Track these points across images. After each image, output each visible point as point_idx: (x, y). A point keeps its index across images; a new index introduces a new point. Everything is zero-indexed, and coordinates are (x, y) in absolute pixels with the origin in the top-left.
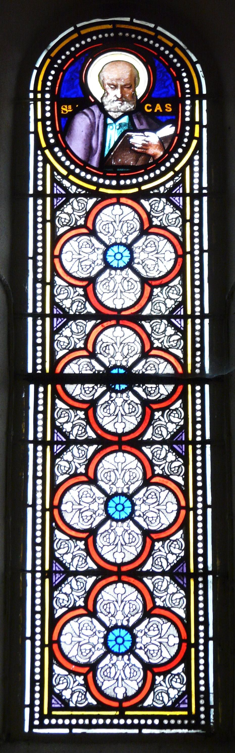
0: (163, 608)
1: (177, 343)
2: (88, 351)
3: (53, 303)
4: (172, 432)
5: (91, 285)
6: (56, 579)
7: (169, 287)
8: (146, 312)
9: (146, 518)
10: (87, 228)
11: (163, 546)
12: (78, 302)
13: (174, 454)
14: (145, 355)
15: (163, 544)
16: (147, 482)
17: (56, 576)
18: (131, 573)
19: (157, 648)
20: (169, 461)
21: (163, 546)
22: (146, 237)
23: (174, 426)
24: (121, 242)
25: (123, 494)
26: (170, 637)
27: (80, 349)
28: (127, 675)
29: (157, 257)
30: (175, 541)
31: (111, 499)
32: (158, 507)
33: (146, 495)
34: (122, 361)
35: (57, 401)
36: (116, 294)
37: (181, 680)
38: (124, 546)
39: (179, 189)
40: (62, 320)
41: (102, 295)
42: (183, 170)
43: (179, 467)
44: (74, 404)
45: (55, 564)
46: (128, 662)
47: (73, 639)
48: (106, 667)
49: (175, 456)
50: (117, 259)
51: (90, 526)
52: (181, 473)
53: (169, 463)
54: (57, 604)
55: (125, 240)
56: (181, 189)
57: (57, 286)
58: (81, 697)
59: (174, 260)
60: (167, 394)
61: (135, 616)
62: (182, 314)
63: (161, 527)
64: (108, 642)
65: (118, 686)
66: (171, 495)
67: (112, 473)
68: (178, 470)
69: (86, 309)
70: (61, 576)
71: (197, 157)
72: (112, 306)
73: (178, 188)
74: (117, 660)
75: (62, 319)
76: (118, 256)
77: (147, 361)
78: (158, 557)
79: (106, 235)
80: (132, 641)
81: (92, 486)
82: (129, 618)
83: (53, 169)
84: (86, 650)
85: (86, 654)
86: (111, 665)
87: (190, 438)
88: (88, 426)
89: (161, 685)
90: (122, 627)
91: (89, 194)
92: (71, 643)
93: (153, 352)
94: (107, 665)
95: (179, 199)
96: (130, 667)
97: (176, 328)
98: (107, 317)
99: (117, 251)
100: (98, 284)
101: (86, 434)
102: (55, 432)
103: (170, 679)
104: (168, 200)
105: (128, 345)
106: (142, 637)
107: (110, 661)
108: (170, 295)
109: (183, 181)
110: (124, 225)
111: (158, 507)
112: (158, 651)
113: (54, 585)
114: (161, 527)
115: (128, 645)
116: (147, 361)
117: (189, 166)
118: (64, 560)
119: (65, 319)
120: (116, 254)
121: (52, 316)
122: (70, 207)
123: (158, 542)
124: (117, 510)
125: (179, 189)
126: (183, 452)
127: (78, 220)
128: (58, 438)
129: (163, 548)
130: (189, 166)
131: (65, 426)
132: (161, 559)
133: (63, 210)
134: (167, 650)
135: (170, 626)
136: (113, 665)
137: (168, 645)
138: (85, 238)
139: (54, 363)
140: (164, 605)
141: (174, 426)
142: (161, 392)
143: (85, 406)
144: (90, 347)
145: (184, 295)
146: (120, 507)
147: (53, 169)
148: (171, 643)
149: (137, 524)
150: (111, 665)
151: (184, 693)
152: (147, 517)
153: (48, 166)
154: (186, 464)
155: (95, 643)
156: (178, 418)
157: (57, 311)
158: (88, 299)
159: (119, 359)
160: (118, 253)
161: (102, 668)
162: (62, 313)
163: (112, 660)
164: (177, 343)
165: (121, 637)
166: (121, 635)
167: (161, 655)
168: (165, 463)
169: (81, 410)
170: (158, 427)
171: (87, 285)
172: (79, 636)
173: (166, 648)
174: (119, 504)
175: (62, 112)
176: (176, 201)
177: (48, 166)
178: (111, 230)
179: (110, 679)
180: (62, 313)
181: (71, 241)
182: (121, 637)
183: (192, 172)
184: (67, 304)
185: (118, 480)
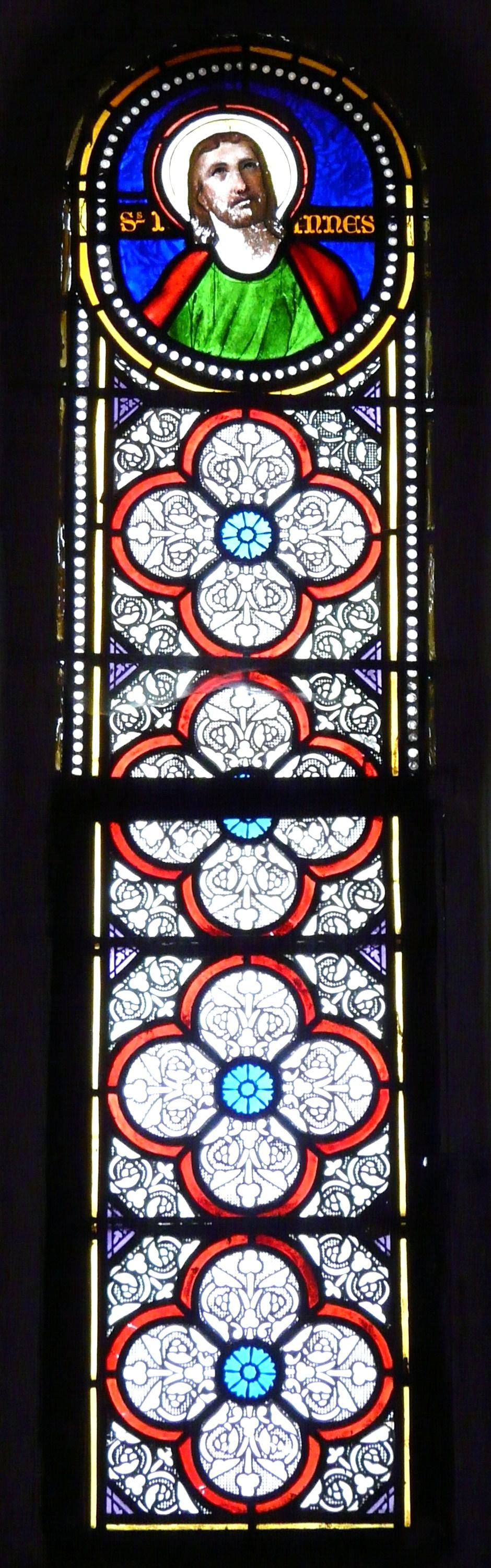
0: (333, 735)
1: (368, 721)
2: (183, 473)
3: (108, 630)
4: (353, 648)
5: (189, 595)
6: (117, 963)
7: (350, 603)
8: (303, 654)
9: (302, 555)
10: (181, 1156)
11: (334, 614)
12: (161, 632)
13: (359, 691)
14: (300, 746)
15: (335, 610)
16: (301, 484)
17: (113, 1236)
18: (273, 1228)
19: (320, 549)
20: (349, 704)
21: (334, 614)
22: (311, 1327)
23: (358, 636)
24: (256, 1407)
25: (253, 508)
26: (345, 526)
27: (168, 470)
28: (262, 1159)
29: (329, 533)
30: (366, 883)
31: (230, 1071)
32: (326, 533)
33: (300, 509)
34: (252, 758)
35: (116, 581)
36: (241, 615)
37: (367, 613)
38: (257, 613)
39: (375, 653)
40: (126, 669)
41: (211, 617)
42: (381, 351)
43: (369, 717)
44: (153, 872)
45: (114, 644)
46: (267, 1421)
47: (154, 533)
48: (220, 1430)
49: (360, 694)
50: (245, 1097)
51: (186, 572)
52: (373, 728)
53: (348, 708)
54: (120, 464)
55: (260, 761)
56: (378, 391)
57: (118, 597)
58: (168, 641)
59: (370, 1098)
60: (349, 565)
61: (279, 487)
62: (379, 658)
63: (332, 572)
64: (224, 1092)
65: (243, 1472)
66: (351, 509)
67: (232, 465)
68: (367, 723)
69: (179, 646)
70: (124, 1236)
71: (392, 348)
72: (231, 639)
73: (373, 389)
74: (243, 1417)
75: (127, 665)
76: (250, 1371)
77: (304, 496)
78: (324, 635)
79: (221, 1037)
80: (277, 1374)
81: (190, 493)
82: (267, 490)
83: (114, 350)
84: (177, 1395)
85: (179, 1120)
86: (229, 1427)
87: (394, 657)
88: (181, 633)
89: (333, 903)
90: (253, 508)
91: (180, 400)
92: (149, 542)
93: (317, 742)
94: (222, 1426)
95: (375, 413)
96: (269, 1432)
97: (366, 430)
98: (224, 665)
99: (245, 546)
100: (203, 593)
101: (177, 648)
102: (106, 1495)
103: (352, 890)
104: (352, 416)
105: (269, 463)
106: (288, 529)
107: (228, 1417)
108: (353, 620)
109: (382, 374)
110: (260, 468)
111: (326, 533)
112: (324, 554)
113: (112, 640)
114: (332, 572)
115: (268, 1381)
116: (304, 496)
117: (393, 342)
118: (130, 637)
119: (134, 667)
120: (243, 1367)
121: (109, 394)
122: (143, 429)
123: (336, 1448)
124: (242, 541)
125: (374, 392)
126: (378, 687)
127: (161, 458)
128: (115, 1507)
129: (340, 897)
130: (393, 342)
131: (130, 1482)
132: (338, 1194)
133: (129, 435)
134: (347, 1107)
135: (345, 505)
136: (233, 1425)
137: (343, 542)
138: (179, 493)
139: (109, 759)
140: (336, 727)
141: (358, 636)
142: (336, 562)
143: (174, 1151)
144: (188, 467)
145: (384, 620)
146: (247, 535)
147: (114, 350)
148: (358, 1380)
149: (282, 567)
150: (229, 1427)
151: (374, 639)
152: (303, 552)
153: (102, 343)
154: (384, 711)
155: (198, 539)
156: (366, 620)
157: (116, 648)
158: (182, 625)
159: (245, 757)
160: (250, 1364)
161: (210, 1432)
162: (125, 652)
163: (232, 1416)
164: (368, 721)
165: (251, 541)
166: (253, 1361)
167: (331, 563)
168: (341, 709)
169: (166, 598)
170: (328, 918)
171: (180, 1153)
172: (165, 528)
173: (339, 547)
174: (249, 542)
175: (124, 229)
176: (373, 959)
177: (102, 343)
178: (233, 475)
179: (226, 1456)
180: (125, 652)
181: (147, 501)
182: (251, 541)
183: (402, 351)
184: (138, 635)
185: (245, 479)
